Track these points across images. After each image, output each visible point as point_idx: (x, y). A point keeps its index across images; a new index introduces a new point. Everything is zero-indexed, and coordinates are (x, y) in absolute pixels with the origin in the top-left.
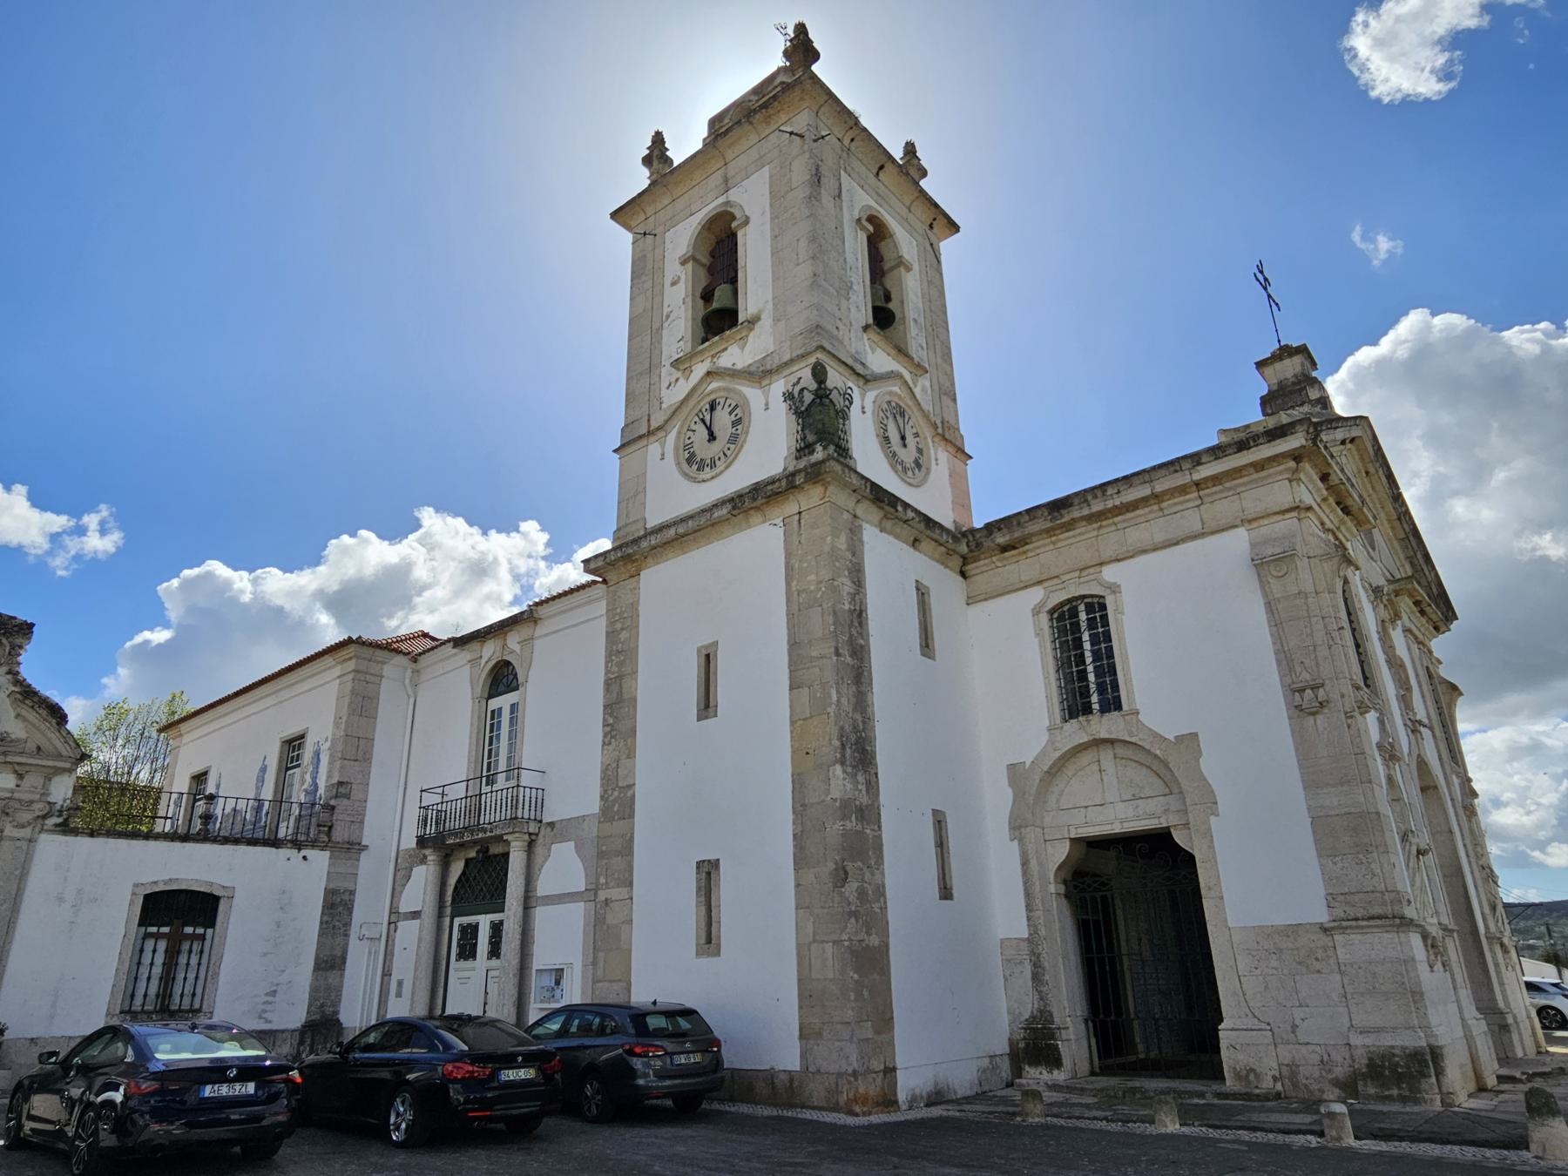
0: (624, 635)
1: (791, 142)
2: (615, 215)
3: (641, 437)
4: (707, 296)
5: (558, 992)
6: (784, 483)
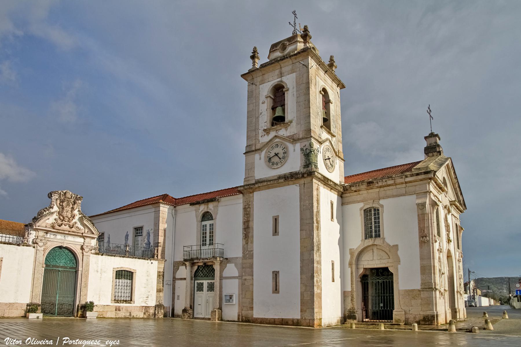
0: (248, 209)
2: (243, 76)
4: (274, 109)
5: (231, 301)
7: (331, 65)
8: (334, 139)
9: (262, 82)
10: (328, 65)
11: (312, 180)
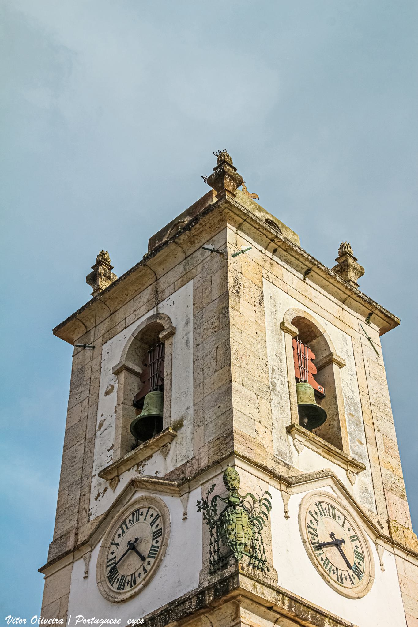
1: (212, 258)
3: (67, 553)
4: (139, 404)
6: (194, 602)
7: (343, 267)
8: (363, 479)
9: (110, 335)
10: (334, 269)
11: (237, 615)
